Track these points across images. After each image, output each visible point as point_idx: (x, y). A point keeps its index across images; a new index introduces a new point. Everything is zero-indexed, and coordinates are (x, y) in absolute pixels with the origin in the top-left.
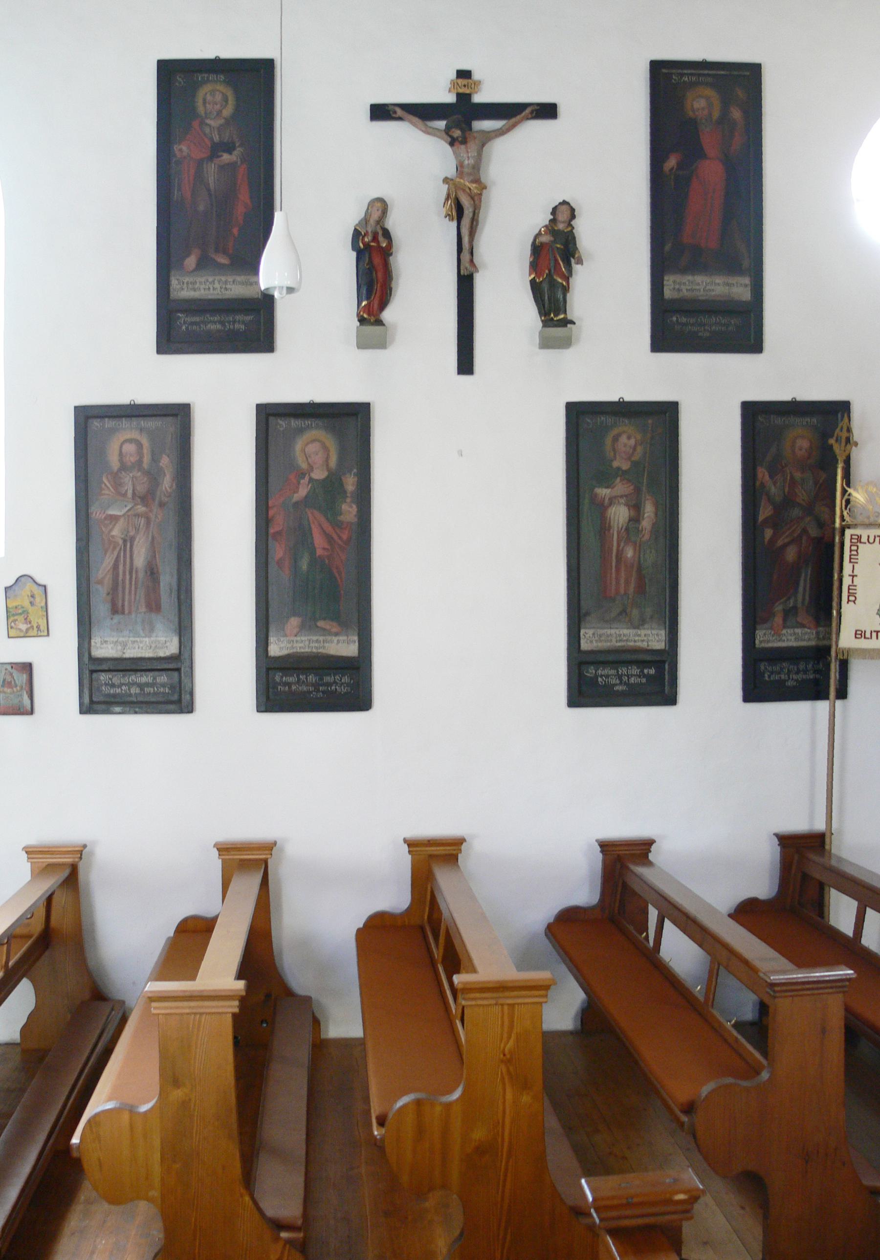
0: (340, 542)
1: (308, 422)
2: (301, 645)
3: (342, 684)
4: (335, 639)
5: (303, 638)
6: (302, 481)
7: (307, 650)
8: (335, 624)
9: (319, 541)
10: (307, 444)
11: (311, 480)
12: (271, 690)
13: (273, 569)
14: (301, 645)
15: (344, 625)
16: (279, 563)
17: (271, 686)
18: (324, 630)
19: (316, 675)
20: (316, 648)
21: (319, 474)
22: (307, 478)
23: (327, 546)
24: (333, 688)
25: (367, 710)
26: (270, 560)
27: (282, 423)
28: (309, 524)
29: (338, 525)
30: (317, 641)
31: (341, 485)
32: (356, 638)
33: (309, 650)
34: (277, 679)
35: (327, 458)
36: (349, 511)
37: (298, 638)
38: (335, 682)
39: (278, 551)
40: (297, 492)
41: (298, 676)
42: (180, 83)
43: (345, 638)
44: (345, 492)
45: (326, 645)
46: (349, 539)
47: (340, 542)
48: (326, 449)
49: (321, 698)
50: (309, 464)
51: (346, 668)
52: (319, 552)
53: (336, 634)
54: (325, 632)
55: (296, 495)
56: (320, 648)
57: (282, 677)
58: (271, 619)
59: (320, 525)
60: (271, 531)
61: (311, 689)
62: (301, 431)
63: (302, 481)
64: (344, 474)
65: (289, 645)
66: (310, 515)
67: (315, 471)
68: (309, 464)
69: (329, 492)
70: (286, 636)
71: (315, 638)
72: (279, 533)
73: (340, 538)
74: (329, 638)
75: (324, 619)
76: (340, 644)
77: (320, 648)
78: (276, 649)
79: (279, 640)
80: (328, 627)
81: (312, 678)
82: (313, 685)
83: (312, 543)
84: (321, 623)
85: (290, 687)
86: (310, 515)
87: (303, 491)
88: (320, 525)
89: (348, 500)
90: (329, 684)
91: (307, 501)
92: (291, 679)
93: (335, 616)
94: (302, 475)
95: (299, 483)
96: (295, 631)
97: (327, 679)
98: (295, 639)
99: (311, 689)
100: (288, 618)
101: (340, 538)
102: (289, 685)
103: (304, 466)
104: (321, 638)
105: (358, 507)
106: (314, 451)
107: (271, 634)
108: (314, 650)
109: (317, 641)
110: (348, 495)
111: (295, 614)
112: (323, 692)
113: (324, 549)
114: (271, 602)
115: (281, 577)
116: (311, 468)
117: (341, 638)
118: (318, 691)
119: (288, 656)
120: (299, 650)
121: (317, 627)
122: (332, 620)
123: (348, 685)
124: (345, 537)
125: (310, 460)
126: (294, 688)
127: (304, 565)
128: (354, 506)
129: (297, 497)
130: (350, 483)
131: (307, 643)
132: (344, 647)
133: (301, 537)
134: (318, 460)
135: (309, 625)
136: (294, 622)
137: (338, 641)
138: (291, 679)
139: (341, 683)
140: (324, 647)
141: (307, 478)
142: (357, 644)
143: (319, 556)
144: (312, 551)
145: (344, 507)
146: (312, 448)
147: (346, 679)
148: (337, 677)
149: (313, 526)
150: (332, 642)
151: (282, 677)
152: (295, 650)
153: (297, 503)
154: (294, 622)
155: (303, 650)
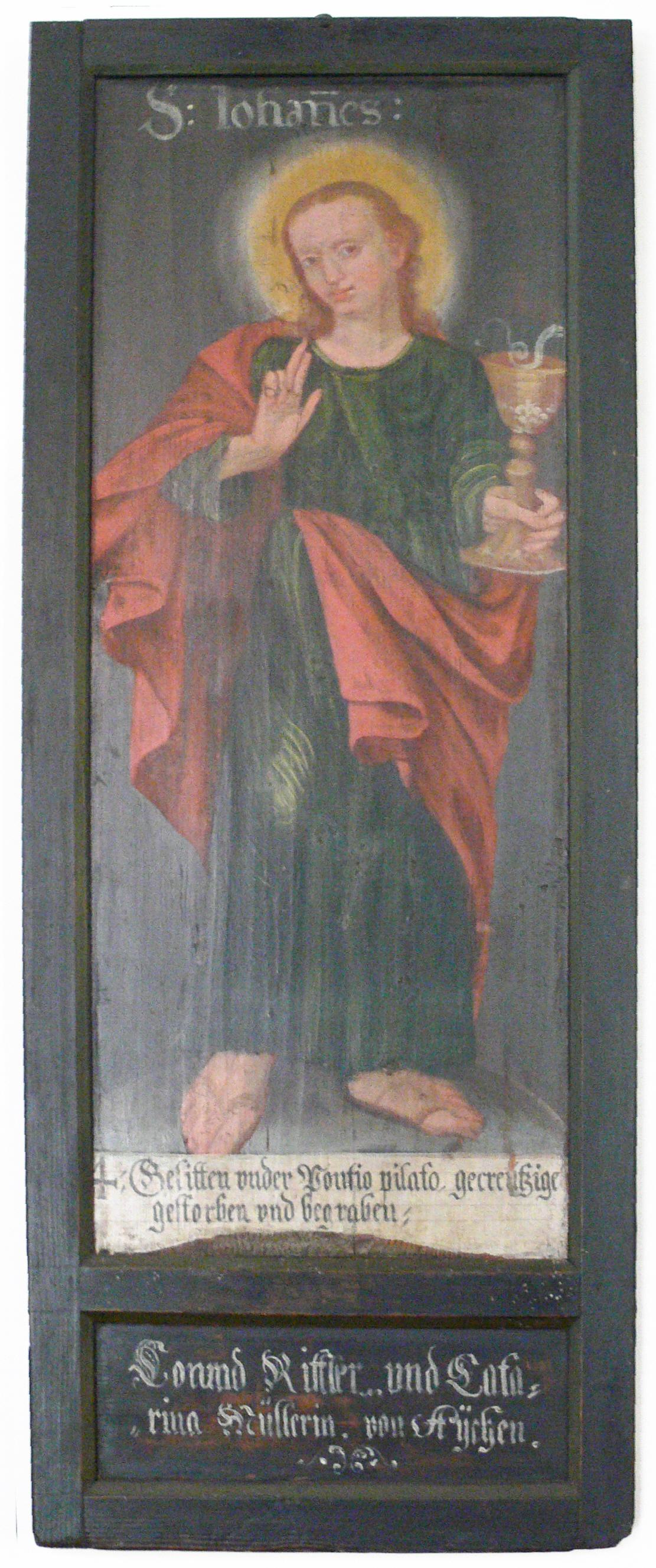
0: (470, 672)
1: (305, 105)
2: (269, 1197)
3: (482, 1403)
4: (446, 1168)
5: (276, 1163)
6: (270, 378)
7: (297, 1224)
8: (443, 1088)
9: (364, 674)
10: (303, 204)
11: (319, 371)
12: (109, 1430)
13: (113, 805)
14: (269, 1197)
15: (496, 1100)
16: (152, 780)
17: (109, 1404)
18: (393, 1119)
19: (345, 1353)
20: (352, 1214)
21: (364, 345)
22: (299, 362)
23: (401, 694)
24: (435, 1422)
25: (611, 1542)
26: (99, 763)
27: (169, 108)
28: (312, 590)
29: (475, 596)
30: (351, 1178)
31: (483, 396)
32: (555, 1165)
33: (312, 1226)
34: (143, 1369)
35: (408, 271)
36: (519, 525)
37: (252, 1163)
38: (445, 1394)
39: (140, 715)
40: (247, 430)
41: (252, 1360)
42: (374, 118)
43: (498, 1163)
44: (505, 433)
45: (401, 1199)
46: (519, 671)
47: (470, 672)
48: (394, 220)
49: (369, 1475)
50: (310, 296)
51: (510, 1323)
52: (363, 724)
53: (454, 1144)
54: (392, 1128)
55: (237, 443)
56: (368, 1212)
57: (166, 1363)
58: (104, 1061)
59: (371, 595)
60: (108, 617)
61: (323, 1426)
62: (262, 145)
63: (270, 378)
64: (497, 345)
65: (203, 1198)
66: (316, 545)
67: (339, 332)
68: (310, 296)
69: (411, 428)
70: (185, 1146)
71: (338, 1163)
72: (152, 627)
73: (475, 656)
74: (416, 1163)
75: (391, 1065)
76: (473, 1197)
77: (368, 1212)
78: (134, 1215)
79: (149, 1170)
80: (408, 1107)
81: (325, 1373)
82: (328, 1406)
83: (329, 679)
84: (367, 1088)
85: (208, 1417)
86: (316, 545)
87: (278, 425)
88: (371, 595)
89: (518, 469)
90: (415, 1405)
91: (295, 474)
92: (213, 1375)
93: (447, 1053)
94: (278, 348)
95: (256, 388)
96: (234, 1126)
97: (402, 1376)
98: (235, 1164)
99: (323, 1426)
100: (197, 1056)
101: (475, 656)
102: (204, 1401)
103: (285, 306)
104: (373, 1164)
105: (567, 502)
106: (337, 242)
107: (105, 1135)
108: (338, 1226)
109: (351, 1178)
110: (521, 445)
111: (231, 1042)
112: (386, 1445)
113: (388, 707)
114: (105, 975)
115: (163, 862)
116: (322, 316)
117: (477, 1164)
118: (359, 1437)
119: (200, 1251)
120: (255, 1226)
121: (353, 1104)
122: (431, 1068)
123: (513, 1407)
124: (498, 650)
125: (314, 279)
126: (228, 1418)
127: (283, 785)
128: (550, 501)
129: (242, 454)
130: (529, 388)
131: (299, 1184)
132: (501, 1210)
133: (270, 640)
134: (360, 273)
135: (310, 1091)
136: (232, 1077)
137: (463, 1182)
138: (213, 1375)
139: (474, 1401)
140: (388, 1211)
141: (299, 362)
142: (560, 1195)
143: (363, 742)
144: (327, 718)
145: (498, 503)
146: (323, 224)
147: (502, 1379)
148: (457, 1366)
149: (329, 595)
150: (425, 1182)
151: (166, 1363)
152: (235, 1226)
153: (245, 480)
154: (232, 1077)
155: (277, 1226)
